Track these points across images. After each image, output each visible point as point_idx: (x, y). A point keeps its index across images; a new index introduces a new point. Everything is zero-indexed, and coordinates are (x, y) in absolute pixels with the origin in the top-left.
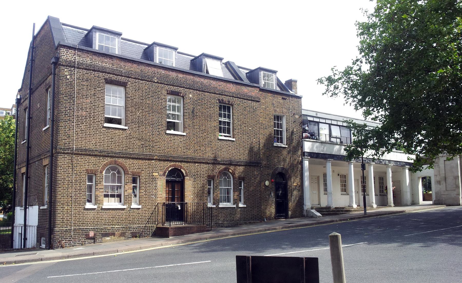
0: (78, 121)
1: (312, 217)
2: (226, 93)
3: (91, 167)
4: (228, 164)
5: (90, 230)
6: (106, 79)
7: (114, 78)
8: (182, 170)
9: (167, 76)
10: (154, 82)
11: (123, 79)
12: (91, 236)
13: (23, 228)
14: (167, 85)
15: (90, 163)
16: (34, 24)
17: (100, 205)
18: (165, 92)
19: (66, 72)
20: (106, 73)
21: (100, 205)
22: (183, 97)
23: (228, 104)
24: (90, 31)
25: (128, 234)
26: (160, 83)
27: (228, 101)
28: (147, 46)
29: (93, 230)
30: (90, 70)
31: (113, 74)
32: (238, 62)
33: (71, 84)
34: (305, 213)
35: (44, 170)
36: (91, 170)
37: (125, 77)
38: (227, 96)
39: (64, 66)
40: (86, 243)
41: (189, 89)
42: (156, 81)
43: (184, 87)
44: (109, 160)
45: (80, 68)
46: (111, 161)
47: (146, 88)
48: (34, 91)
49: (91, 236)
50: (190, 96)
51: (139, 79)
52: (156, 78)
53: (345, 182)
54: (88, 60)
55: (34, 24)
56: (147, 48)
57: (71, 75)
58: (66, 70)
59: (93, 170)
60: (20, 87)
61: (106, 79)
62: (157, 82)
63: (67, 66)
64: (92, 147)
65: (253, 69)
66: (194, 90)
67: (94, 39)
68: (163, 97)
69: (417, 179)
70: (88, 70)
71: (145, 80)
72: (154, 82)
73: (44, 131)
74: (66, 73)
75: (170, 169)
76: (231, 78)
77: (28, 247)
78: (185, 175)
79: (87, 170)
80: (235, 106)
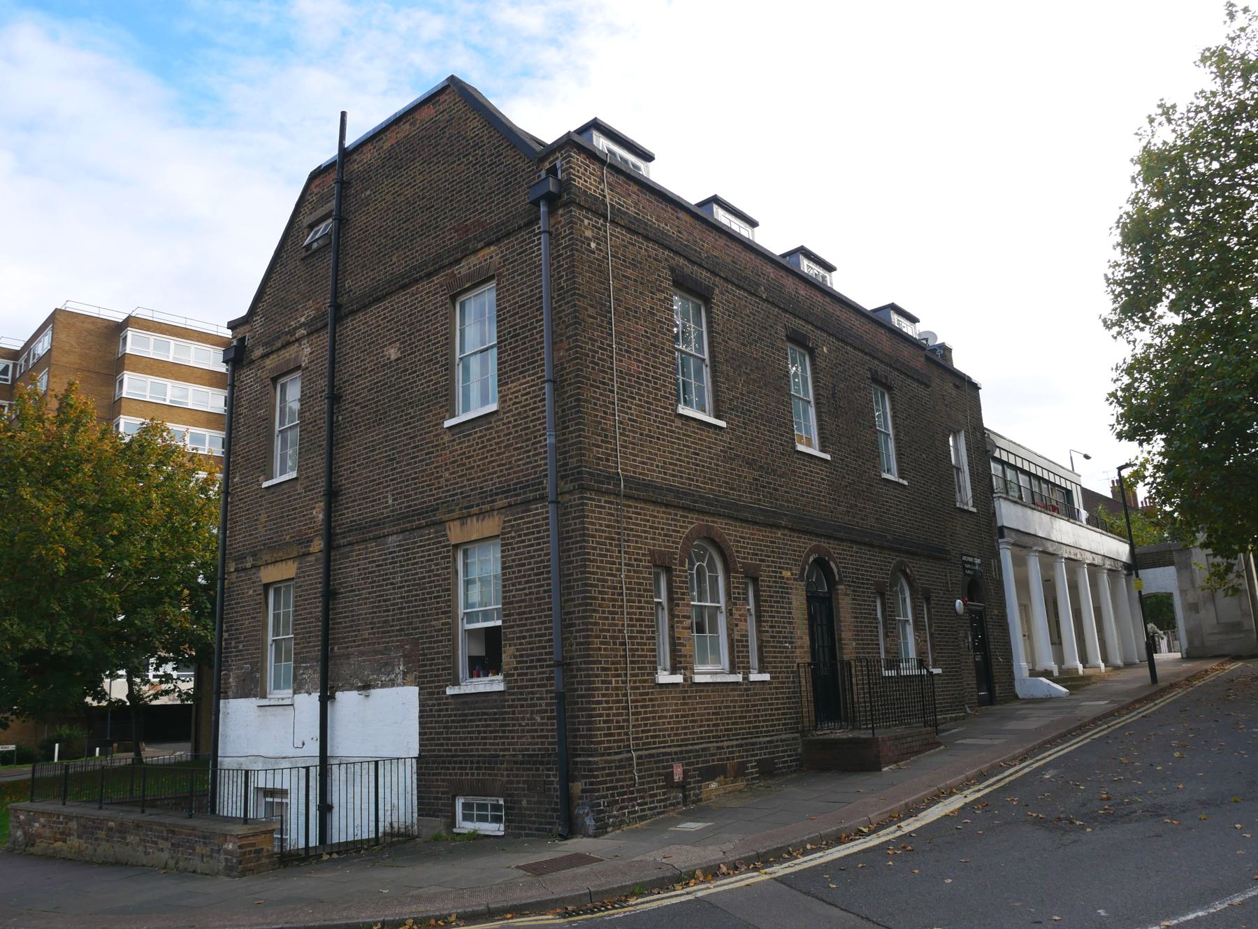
5: (673, 760)
8: (832, 564)
13: (314, 773)
16: (343, 114)
18: (782, 333)
19: (586, 228)
25: (752, 770)
29: (679, 757)
31: (686, 258)
33: (601, 270)
35: (455, 560)
39: (581, 207)
48: (346, 316)
55: (343, 114)
60: (242, 311)
62: (766, 300)
63: (589, 210)
64: (656, 477)
73: (450, 428)
74: (588, 234)
75: (811, 559)
77: (335, 840)
79: (652, 553)
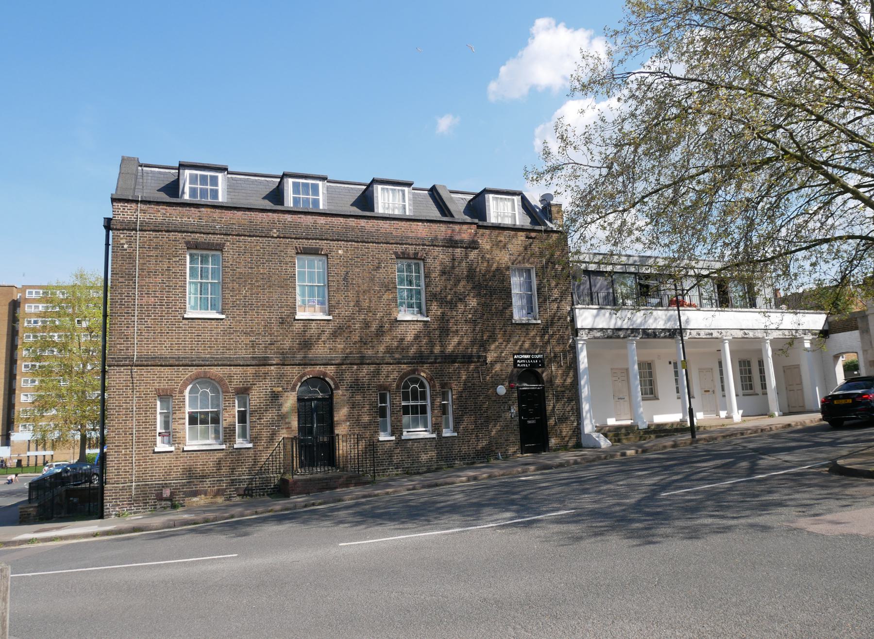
0: (141, 313)
1: (596, 446)
2: (409, 241)
3: (164, 385)
4: (417, 363)
6: (187, 243)
7: (312, 244)
8: (327, 379)
9: (297, 226)
10: (272, 237)
11: (216, 239)
12: (165, 496)
14: (296, 238)
15: (163, 377)
17: (181, 446)
20: (187, 232)
21: (181, 446)
22: (326, 255)
23: (415, 258)
24: (370, 186)
26: (284, 238)
27: (402, 253)
28: (364, 187)
30: (162, 231)
32: (446, 183)
34: (584, 442)
36: (163, 390)
37: (221, 234)
38: (412, 244)
40: (158, 507)
41: (338, 240)
42: (275, 235)
43: (327, 240)
44: (194, 370)
45: (145, 231)
46: (199, 373)
47: (258, 248)
49: (165, 496)
50: (340, 252)
51: (245, 236)
52: (275, 231)
53: (750, 381)
54: (176, 216)
56: (366, 190)
57: (130, 243)
58: (122, 236)
59: (167, 389)
61: (187, 243)
62: (278, 237)
63: (123, 230)
65: (479, 192)
66: (347, 241)
67: (375, 195)
68: (288, 259)
69: (831, 360)
70: (158, 231)
71: (256, 236)
72: (272, 237)
76: (435, 214)
78: (333, 386)
80: (428, 260)
